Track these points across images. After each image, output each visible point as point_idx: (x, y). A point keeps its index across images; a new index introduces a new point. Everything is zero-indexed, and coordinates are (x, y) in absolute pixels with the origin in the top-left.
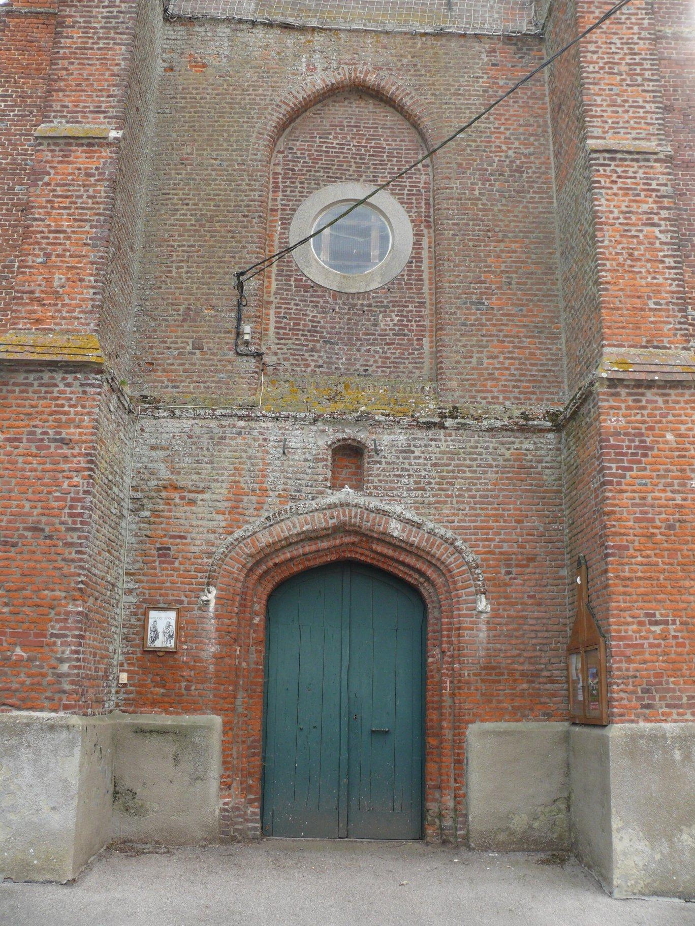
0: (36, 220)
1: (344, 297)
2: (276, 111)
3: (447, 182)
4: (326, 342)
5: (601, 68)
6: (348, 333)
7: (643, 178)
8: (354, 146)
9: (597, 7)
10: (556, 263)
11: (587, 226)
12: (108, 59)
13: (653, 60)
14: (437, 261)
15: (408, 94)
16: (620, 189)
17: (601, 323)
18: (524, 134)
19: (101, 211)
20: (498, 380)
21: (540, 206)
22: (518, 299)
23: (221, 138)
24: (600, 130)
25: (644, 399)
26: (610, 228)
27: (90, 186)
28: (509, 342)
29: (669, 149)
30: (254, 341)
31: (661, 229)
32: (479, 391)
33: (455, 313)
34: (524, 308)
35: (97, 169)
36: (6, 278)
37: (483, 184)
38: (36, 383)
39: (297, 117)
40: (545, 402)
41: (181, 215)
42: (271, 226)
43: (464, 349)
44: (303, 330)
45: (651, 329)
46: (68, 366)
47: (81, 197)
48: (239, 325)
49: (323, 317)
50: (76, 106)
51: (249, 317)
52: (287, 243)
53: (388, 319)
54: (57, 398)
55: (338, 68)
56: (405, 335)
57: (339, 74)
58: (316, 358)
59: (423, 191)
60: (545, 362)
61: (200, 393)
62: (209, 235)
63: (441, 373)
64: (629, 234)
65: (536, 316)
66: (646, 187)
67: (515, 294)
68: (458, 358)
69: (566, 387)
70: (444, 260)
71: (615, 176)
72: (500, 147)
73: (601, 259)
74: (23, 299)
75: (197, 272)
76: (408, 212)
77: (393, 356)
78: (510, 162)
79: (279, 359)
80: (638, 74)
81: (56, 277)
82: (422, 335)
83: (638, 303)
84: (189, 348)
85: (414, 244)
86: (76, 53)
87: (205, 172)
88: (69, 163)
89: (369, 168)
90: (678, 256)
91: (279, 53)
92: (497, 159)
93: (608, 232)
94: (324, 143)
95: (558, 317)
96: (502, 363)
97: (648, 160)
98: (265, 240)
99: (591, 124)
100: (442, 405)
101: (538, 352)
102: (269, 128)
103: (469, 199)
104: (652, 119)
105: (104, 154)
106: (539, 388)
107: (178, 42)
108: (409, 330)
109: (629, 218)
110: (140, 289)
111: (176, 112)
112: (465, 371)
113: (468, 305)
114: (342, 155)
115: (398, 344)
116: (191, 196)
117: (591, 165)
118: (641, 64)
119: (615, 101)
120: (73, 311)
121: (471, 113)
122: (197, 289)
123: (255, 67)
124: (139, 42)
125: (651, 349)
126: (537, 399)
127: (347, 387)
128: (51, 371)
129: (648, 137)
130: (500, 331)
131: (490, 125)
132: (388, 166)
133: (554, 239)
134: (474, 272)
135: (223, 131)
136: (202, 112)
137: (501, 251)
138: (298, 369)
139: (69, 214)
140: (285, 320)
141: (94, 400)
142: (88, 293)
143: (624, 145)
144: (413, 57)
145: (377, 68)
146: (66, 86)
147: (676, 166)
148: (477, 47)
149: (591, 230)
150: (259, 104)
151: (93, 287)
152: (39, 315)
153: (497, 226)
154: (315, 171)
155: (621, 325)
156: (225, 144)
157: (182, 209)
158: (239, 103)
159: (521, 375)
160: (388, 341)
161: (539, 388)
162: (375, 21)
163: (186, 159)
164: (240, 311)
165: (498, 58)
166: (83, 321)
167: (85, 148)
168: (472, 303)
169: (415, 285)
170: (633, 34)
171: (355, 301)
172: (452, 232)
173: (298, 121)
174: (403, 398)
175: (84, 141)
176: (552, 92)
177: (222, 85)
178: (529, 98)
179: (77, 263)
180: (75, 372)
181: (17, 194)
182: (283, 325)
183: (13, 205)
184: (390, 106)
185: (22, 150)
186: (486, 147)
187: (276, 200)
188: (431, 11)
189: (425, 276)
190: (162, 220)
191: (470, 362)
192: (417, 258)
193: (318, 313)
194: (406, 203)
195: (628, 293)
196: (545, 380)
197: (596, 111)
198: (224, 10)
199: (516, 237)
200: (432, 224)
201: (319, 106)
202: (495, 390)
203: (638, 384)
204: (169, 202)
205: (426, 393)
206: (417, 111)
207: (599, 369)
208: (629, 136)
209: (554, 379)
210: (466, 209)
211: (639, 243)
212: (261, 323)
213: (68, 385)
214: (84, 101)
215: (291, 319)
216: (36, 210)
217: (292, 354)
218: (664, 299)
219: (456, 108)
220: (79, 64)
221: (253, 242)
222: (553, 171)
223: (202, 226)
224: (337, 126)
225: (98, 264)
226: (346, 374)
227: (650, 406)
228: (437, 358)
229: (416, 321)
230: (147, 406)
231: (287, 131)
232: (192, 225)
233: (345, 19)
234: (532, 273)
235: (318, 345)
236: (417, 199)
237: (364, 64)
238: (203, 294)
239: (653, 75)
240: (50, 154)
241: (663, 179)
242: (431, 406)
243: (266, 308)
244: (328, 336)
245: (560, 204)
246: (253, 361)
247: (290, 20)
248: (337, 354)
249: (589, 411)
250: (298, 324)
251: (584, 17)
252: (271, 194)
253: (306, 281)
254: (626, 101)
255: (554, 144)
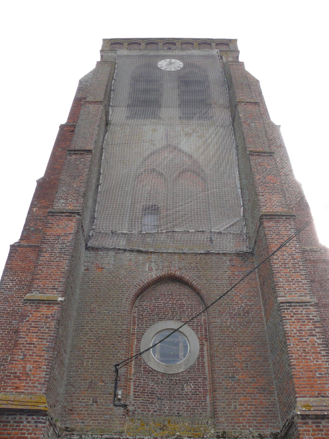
0: (21, 338)
1: (167, 376)
2: (135, 288)
3: (214, 319)
4: (158, 399)
5: (281, 266)
6: (169, 394)
7: (306, 314)
8: (171, 304)
9: (276, 240)
10: (269, 356)
11: (282, 338)
12: (60, 266)
13: (303, 261)
14: (211, 357)
15: (194, 280)
16: (295, 319)
17: (294, 385)
18: (248, 296)
19: (52, 334)
20: (245, 416)
21: (259, 329)
22: (252, 374)
23: (109, 301)
24: (283, 293)
25: (321, 425)
26: (293, 338)
27: (48, 322)
28: (249, 396)
29: (316, 300)
30: (123, 399)
31: (317, 337)
32: (235, 423)
33: (221, 383)
34: (255, 379)
35: (51, 315)
36: (3, 365)
37: (231, 320)
38: (12, 421)
39: (144, 291)
40: (270, 427)
41: (89, 336)
42: (132, 342)
43: (227, 401)
44: (147, 393)
45: (319, 387)
46: (30, 412)
47: (43, 327)
48: (116, 390)
49: (157, 386)
50: (44, 286)
51: (121, 386)
52: (140, 349)
53: (189, 387)
54: (22, 429)
55: (162, 269)
56: (197, 394)
57: (163, 272)
58: (153, 407)
59: (203, 324)
60: (268, 406)
61: (95, 426)
62: (102, 346)
63: (216, 414)
64: (302, 340)
65: (261, 383)
66: (307, 318)
67: (250, 372)
68: (224, 406)
69: (280, 419)
70: (215, 357)
71: (292, 313)
72: (238, 302)
73: (290, 353)
74: (10, 376)
75: (96, 364)
76: (196, 334)
77: (192, 406)
78: (243, 309)
79: (135, 408)
80: (297, 268)
81: (28, 366)
82: (206, 394)
83: (311, 374)
84: (91, 402)
85: (200, 349)
86: (46, 263)
87: (101, 316)
88: (39, 311)
89: (178, 314)
90: (327, 350)
91: (136, 263)
92: (237, 308)
93: (292, 340)
94: (157, 302)
95: (272, 383)
96: (247, 408)
97: (307, 306)
98: (129, 348)
99: (279, 291)
100: (217, 431)
101: (264, 401)
102: (131, 296)
103: (225, 327)
104: (306, 287)
105: (55, 308)
106: (266, 420)
107: (91, 258)
108: (199, 392)
109: (301, 333)
110: (68, 372)
111: (89, 288)
112: (228, 412)
113: (228, 378)
114: (165, 308)
115: (194, 399)
116: (94, 327)
117: (281, 309)
118: (298, 263)
119: (288, 280)
120: (35, 383)
121: (223, 287)
122: (96, 372)
123: (125, 269)
124: (74, 259)
125: (320, 398)
126: (266, 426)
127: (169, 422)
128: (21, 414)
129: (305, 295)
130: (245, 391)
131: (233, 293)
132: (187, 313)
133: (266, 344)
134: (229, 362)
135: (110, 297)
136: (101, 289)
137: (242, 351)
138: (145, 413)
139: (36, 336)
140: (138, 388)
141: (41, 430)
142: (43, 374)
143: (295, 299)
144: (196, 264)
145: (180, 269)
146: (40, 277)
147: (320, 307)
148: (224, 258)
149: (284, 340)
150: (126, 285)
151: (45, 371)
152: (18, 385)
153: (239, 339)
154: (153, 316)
155: (304, 386)
156: (111, 303)
157: (90, 333)
158: (118, 285)
159: (257, 414)
160: (189, 398)
161: (266, 420)
162: (179, 249)
163: (93, 310)
164: (116, 384)
165: (234, 263)
166: (39, 388)
167: (47, 305)
168: (229, 378)
169: (201, 369)
170: (293, 251)
171: (173, 378)
172: (218, 343)
173: (145, 292)
174: (198, 427)
175: (46, 302)
176: (260, 276)
177: (110, 277)
178: (250, 279)
179: (39, 359)
180: (33, 415)
181: (13, 325)
182: (137, 390)
183: (11, 330)
184: (186, 285)
185: (18, 304)
186: (231, 302)
187: (134, 329)
188: (203, 244)
189: (206, 365)
190: (80, 338)
191: (231, 408)
192: (201, 356)
193: (154, 384)
194: (195, 330)
195: (305, 369)
196: (269, 415)
197: (280, 285)
198: (112, 245)
199: (248, 344)
200: (208, 340)
201: (154, 286)
202: (244, 422)
203: (317, 417)
204: (84, 330)
205: (209, 425)
206: (199, 287)
207: (296, 410)
208: (296, 295)
209: (273, 415)
210: (224, 332)
211: (308, 345)
212: (126, 389)
213: (28, 422)
214: (48, 284)
215: (142, 387)
216: (21, 333)
217: (141, 405)
218: (323, 371)
219: (217, 286)
220: (47, 268)
221: (123, 350)
222: (263, 312)
223: (99, 341)
224: (162, 295)
225: (48, 360)
226: (168, 415)
227: (325, 429)
228: (214, 406)
229: (202, 387)
230: (68, 433)
231: (140, 297)
232: (94, 341)
233: (165, 248)
234: (257, 361)
235: (155, 400)
236: (200, 328)
237: (174, 267)
238: (98, 375)
239: (304, 268)
240: (30, 307)
241: (315, 314)
242: (212, 432)
243: (129, 382)
244: (159, 396)
245: (268, 327)
246: (122, 409)
247: (141, 249)
248: (164, 405)
249: (294, 433)
250: (145, 390)
251: (270, 245)
252: (132, 327)
253: (148, 368)
254: (294, 280)
255: (263, 300)
